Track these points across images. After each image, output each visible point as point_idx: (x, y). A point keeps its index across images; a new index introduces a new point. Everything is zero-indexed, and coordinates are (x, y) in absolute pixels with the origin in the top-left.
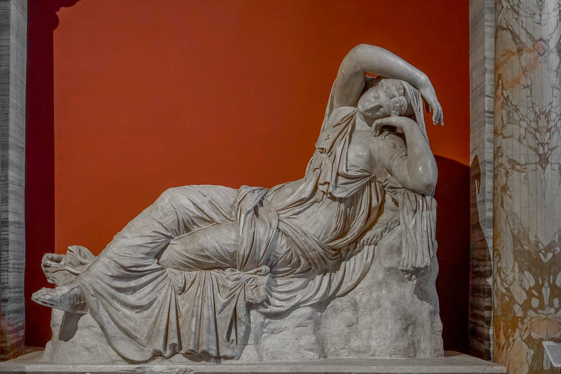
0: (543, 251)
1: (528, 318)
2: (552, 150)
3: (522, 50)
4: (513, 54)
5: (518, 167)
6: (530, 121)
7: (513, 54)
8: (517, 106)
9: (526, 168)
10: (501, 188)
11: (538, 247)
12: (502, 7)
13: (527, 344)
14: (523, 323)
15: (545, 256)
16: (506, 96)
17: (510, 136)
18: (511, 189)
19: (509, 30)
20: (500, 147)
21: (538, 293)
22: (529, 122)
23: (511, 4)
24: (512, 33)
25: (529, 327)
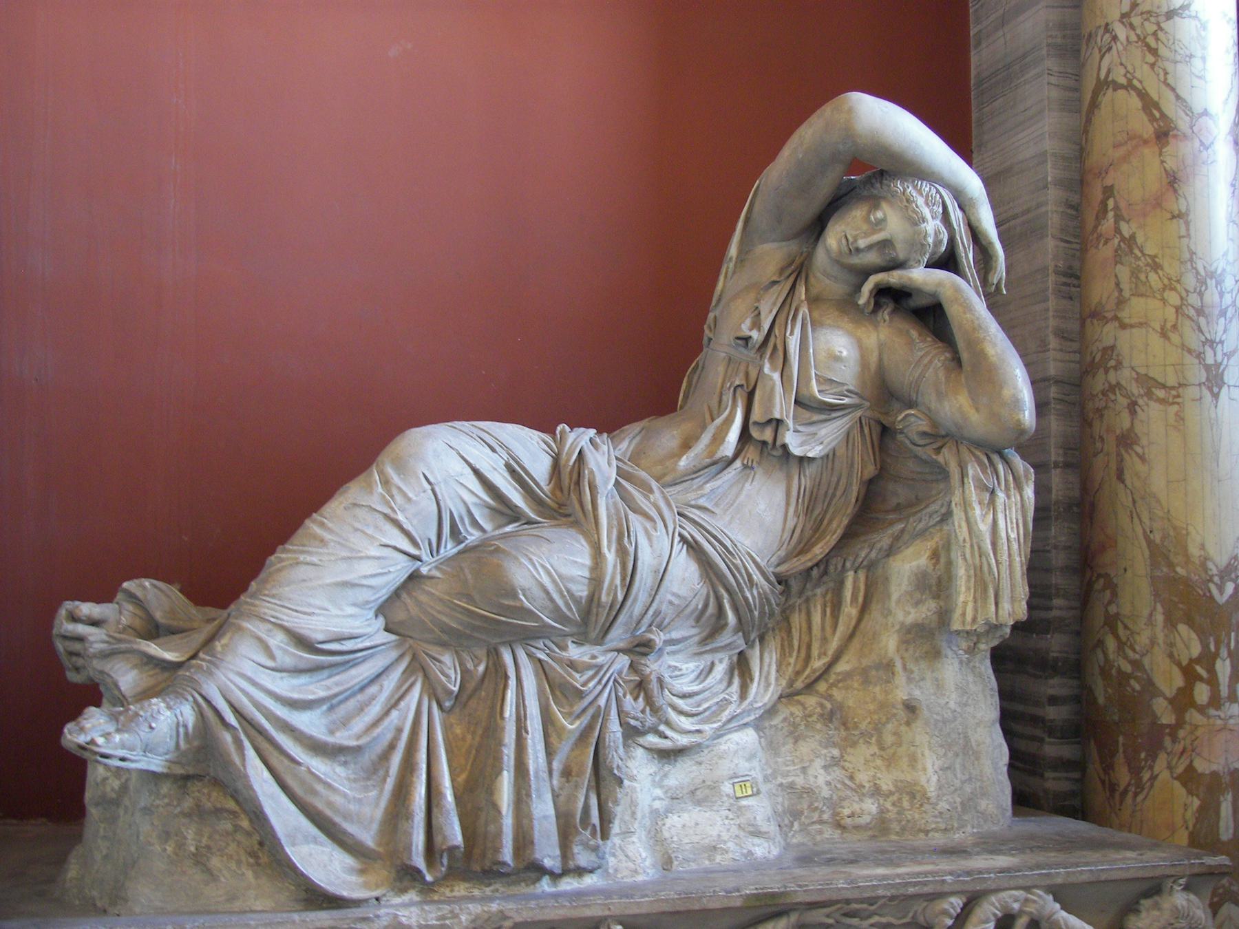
0: (1216, 579)
1: (1188, 727)
2: (1228, 355)
3: (1166, 134)
4: (1146, 142)
5: (1161, 393)
6: (1187, 291)
7: (1146, 142)
8: (1156, 256)
9: (1178, 396)
10: (1117, 438)
11: (1206, 570)
12: (1115, 38)
13: (1184, 784)
14: (1175, 739)
15: (1221, 589)
16: (1127, 236)
17: (1141, 324)
18: (1144, 441)
19: (1134, 88)
20: (1113, 348)
21: (1208, 671)
22: (1184, 294)
23: (1139, 31)
24: (1143, 95)
25: (1189, 747)
